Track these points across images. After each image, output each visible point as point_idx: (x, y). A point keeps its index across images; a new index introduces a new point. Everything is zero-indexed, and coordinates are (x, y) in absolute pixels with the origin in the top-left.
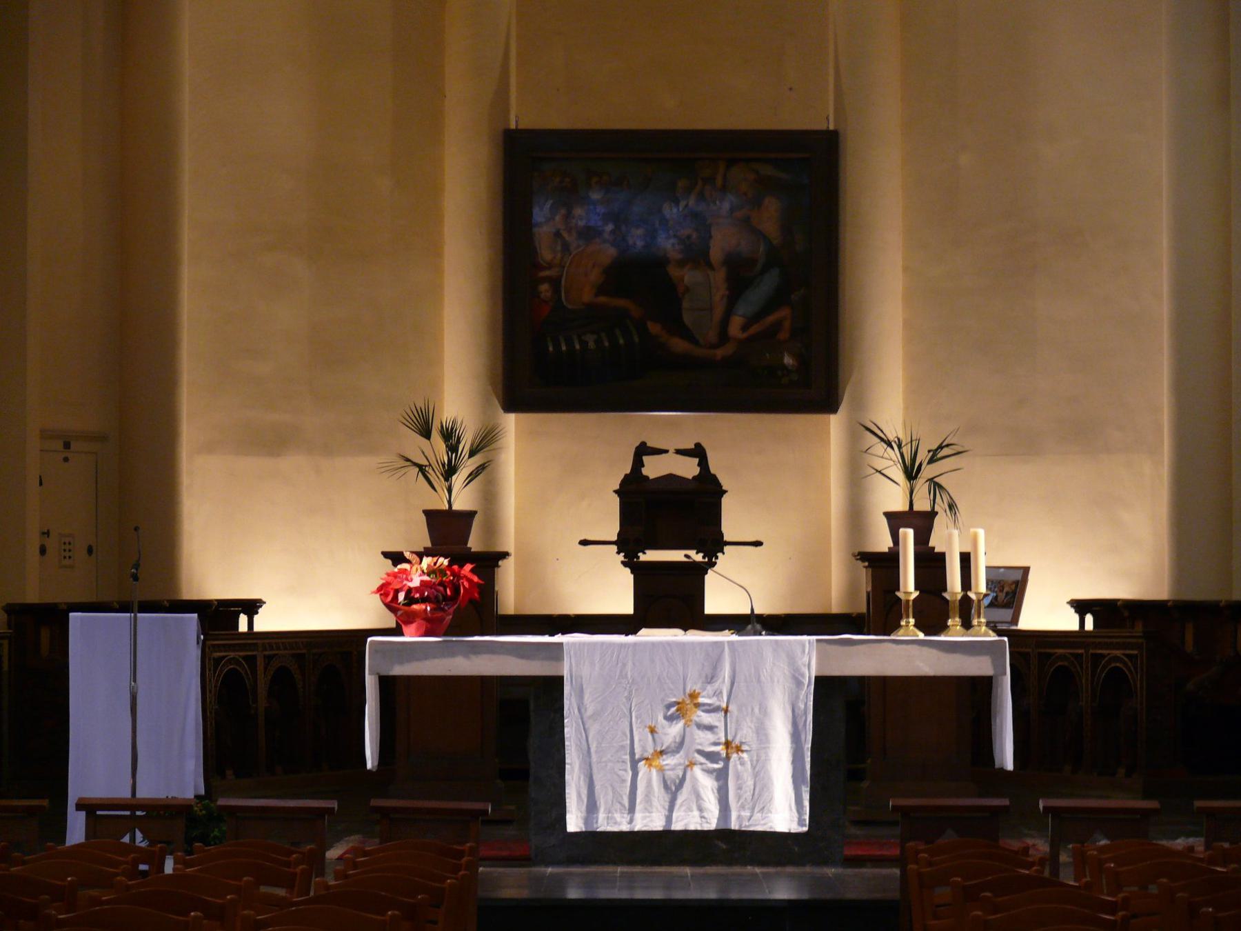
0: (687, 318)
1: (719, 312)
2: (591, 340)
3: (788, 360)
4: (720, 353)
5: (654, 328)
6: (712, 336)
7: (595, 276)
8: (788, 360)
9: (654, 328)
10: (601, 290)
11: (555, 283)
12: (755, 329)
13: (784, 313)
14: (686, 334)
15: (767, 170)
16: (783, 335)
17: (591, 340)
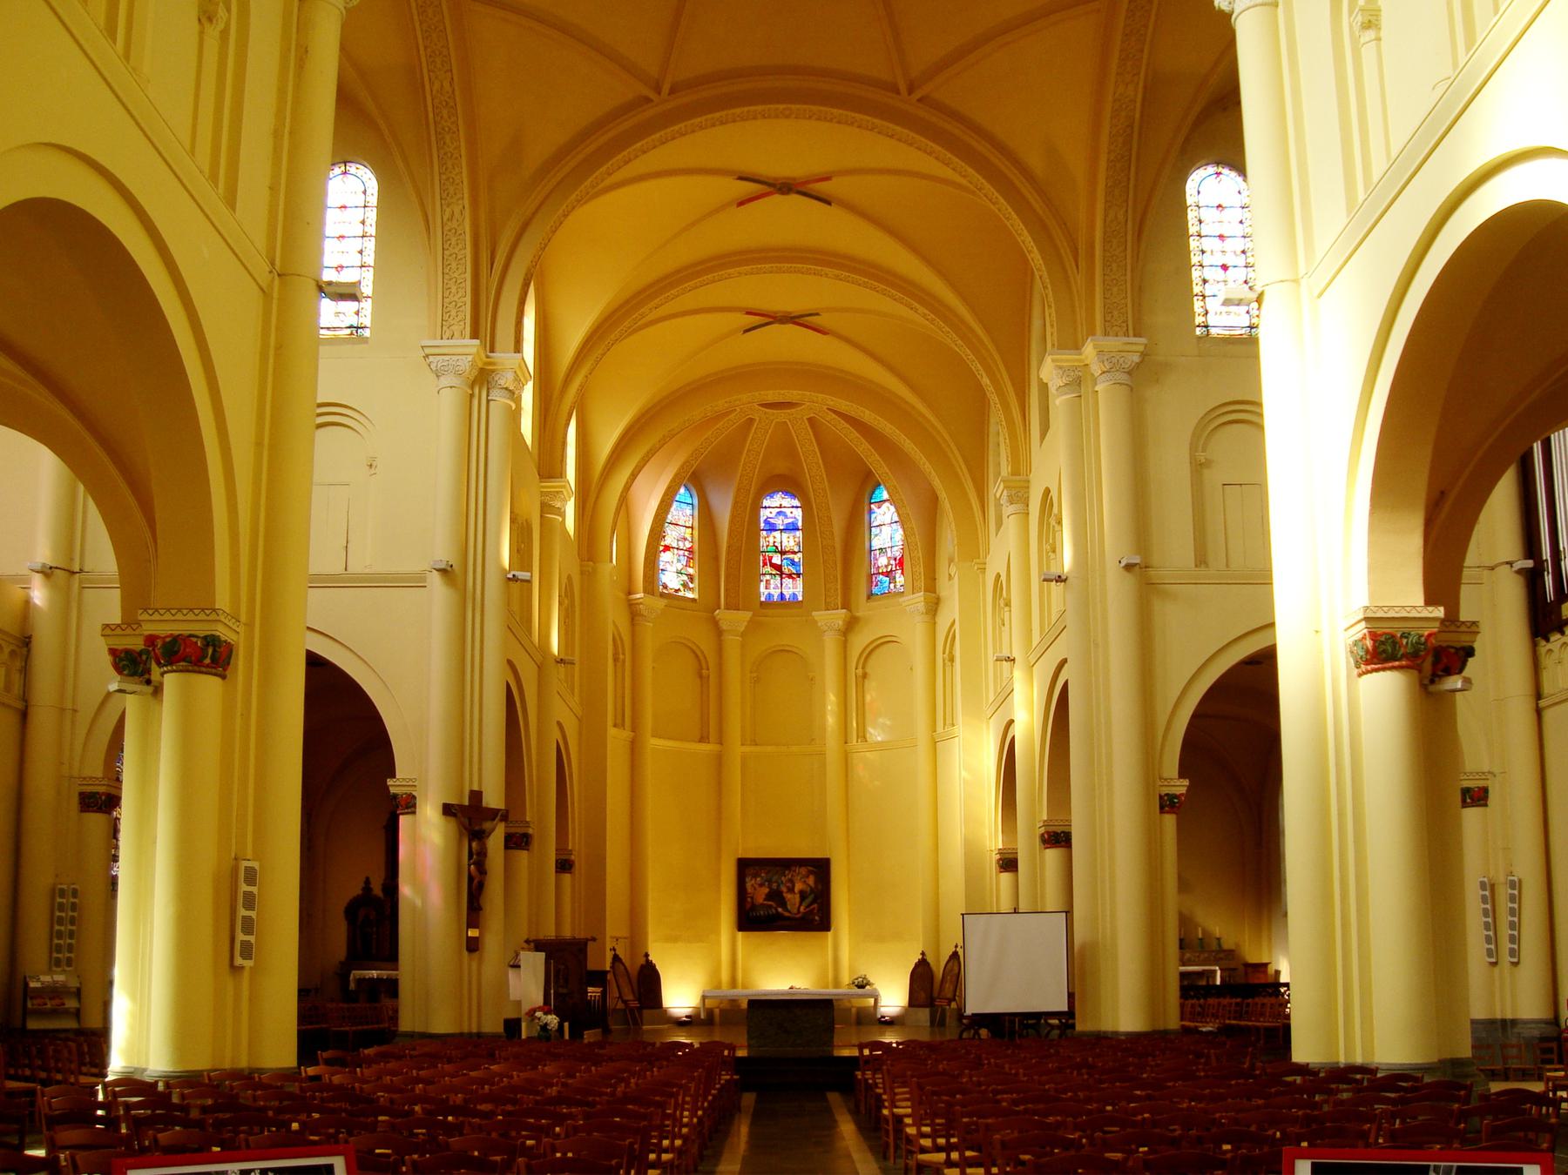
0: (789, 907)
1: (797, 905)
2: (762, 913)
3: (817, 918)
4: (798, 916)
5: (780, 910)
6: (795, 911)
7: (763, 896)
8: (817, 918)
9: (780, 910)
10: (765, 900)
11: (752, 898)
12: (808, 909)
13: (815, 905)
14: (790, 912)
15: (810, 868)
16: (815, 911)
17: (1386, 1125)
